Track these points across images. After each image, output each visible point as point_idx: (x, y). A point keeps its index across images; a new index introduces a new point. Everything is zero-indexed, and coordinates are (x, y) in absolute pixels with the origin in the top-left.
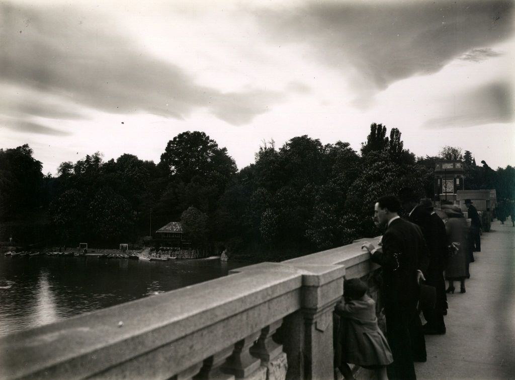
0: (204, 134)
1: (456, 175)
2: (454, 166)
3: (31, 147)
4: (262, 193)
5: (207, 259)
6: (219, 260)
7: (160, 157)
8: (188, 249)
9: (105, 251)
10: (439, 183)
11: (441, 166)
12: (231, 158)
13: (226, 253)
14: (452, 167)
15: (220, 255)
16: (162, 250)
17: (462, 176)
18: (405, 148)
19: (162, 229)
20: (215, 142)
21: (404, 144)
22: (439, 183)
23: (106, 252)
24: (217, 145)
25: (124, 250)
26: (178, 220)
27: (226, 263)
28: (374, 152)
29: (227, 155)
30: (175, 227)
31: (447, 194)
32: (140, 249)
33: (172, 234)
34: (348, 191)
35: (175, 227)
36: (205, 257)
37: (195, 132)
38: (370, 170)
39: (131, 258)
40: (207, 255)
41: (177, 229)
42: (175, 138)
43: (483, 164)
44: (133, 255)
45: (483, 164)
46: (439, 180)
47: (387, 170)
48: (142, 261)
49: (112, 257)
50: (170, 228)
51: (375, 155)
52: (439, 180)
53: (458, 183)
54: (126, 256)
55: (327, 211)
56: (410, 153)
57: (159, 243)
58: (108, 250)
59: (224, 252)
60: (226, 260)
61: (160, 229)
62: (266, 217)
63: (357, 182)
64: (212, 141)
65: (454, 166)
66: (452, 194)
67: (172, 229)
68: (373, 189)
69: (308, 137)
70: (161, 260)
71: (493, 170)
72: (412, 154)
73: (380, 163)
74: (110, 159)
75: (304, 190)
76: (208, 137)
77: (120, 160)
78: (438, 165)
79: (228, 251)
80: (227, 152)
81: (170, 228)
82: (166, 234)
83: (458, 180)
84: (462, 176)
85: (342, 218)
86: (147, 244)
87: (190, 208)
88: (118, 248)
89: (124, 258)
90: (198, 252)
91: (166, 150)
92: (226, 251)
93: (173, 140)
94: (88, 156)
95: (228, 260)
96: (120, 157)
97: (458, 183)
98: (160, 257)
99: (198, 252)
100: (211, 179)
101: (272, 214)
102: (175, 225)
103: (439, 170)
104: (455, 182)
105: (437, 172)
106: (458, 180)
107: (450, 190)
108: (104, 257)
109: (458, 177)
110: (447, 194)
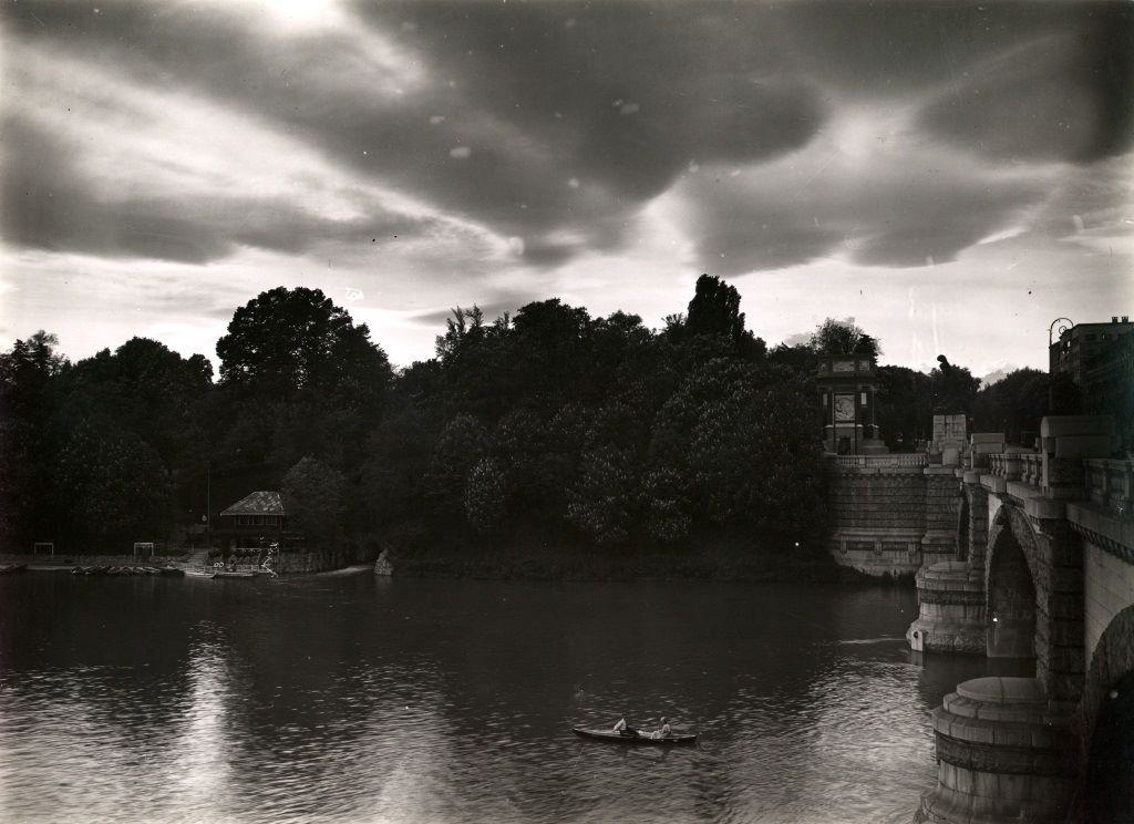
0: (319, 293)
1: (860, 386)
2: (857, 367)
3: (832, 318)
4: (468, 425)
5: (342, 571)
6: (370, 577)
7: (215, 346)
8: (298, 551)
9: (99, 559)
10: (825, 403)
11: (830, 368)
12: (378, 349)
13: (386, 558)
14: (853, 369)
15: (372, 559)
16: (238, 554)
17: (873, 389)
18: (747, 328)
19: (235, 507)
20: (346, 313)
21: (747, 320)
22: (825, 403)
23: (100, 562)
24: (349, 320)
25: (144, 555)
26: (274, 488)
27: (389, 579)
28: (704, 338)
29: (369, 341)
30: (265, 503)
31: (837, 425)
32: (183, 553)
33: (257, 518)
34: (655, 419)
35: (265, 503)
36: (337, 569)
37: (300, 290)
38: (699, 375)
39: (165, 573)
40: (339, 564)
41: (271, 506)
42: (251, 303)
43: (940, 363)
44: (169, 567)
45: (940, 363)
46: (825, 397)
47: (732, 377)
48: (193, 579)
49: (117, 575)
50: (253, 505)
51: (705, 344)
52: (825, 397)
53: (864, 402)
54: (153, 570)
55: (616, 462)
56: (755, 337)
57: (239, 538)
58: (104, 557)
59: (382, 556)
60: (388, 572)
61: (230, 508)
62: (479, 478)
63: (675, 400)
64: (339, 310)
65: (857, 367)
66: (853, 425)
67: (260, 507)
68: (711, 416)
69: (562, 304)
70: (239, 577)
71: (388, 366)
72: (759, 339)
73: (719, 360)
74: (101, 349)
75: (557, 418)
76: (330, 301)
77: (123, 350)
78: (824, 365)
79: (390, 553)
80: (369, 334)
81: (253, 505)
82: (244, 518)
83: (864, 396)
84: (873, 389)
85: (647, 478)
86: (197, 542)
87: (305, 459)
88: (128, 551)
89: (148, 574)
90: (321, 556)
91: (230, 329)
92: (386, 552)
93: (245, 306)
94: (19, 342)
95: (393, 572)
96: (124, 343)
97: (864, 402)
98: (234, 570)
99: (321, 556)
100: (340, 396)
101: (494, 471)
102: (265, 499)
103: (826, 374)
104: (858, 400)
105: (820, 380)
106: (864, 396)
107: (848, 418)
108: (99, 574)
109: (865, 390)
110: (837, 425)
